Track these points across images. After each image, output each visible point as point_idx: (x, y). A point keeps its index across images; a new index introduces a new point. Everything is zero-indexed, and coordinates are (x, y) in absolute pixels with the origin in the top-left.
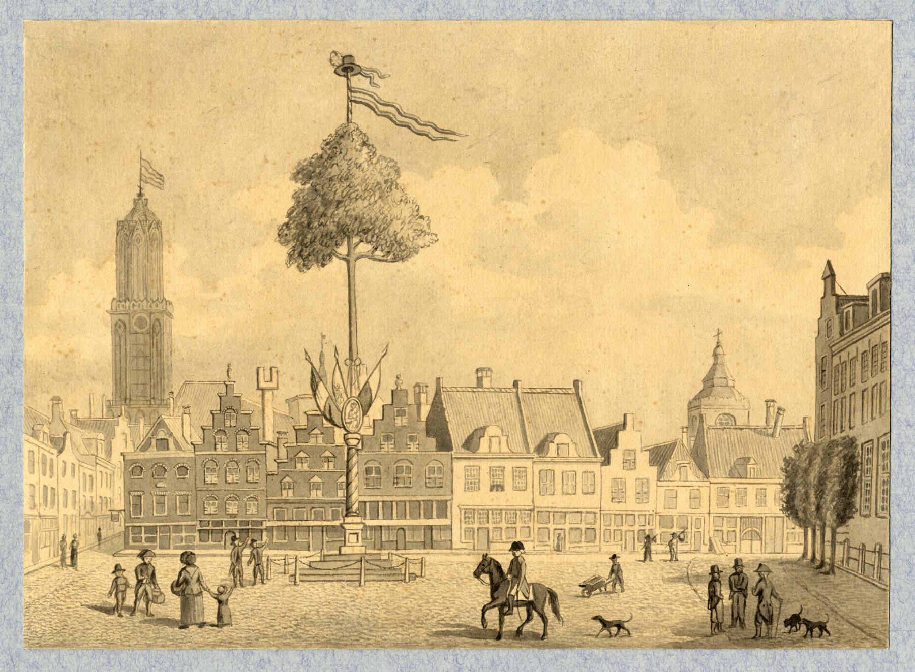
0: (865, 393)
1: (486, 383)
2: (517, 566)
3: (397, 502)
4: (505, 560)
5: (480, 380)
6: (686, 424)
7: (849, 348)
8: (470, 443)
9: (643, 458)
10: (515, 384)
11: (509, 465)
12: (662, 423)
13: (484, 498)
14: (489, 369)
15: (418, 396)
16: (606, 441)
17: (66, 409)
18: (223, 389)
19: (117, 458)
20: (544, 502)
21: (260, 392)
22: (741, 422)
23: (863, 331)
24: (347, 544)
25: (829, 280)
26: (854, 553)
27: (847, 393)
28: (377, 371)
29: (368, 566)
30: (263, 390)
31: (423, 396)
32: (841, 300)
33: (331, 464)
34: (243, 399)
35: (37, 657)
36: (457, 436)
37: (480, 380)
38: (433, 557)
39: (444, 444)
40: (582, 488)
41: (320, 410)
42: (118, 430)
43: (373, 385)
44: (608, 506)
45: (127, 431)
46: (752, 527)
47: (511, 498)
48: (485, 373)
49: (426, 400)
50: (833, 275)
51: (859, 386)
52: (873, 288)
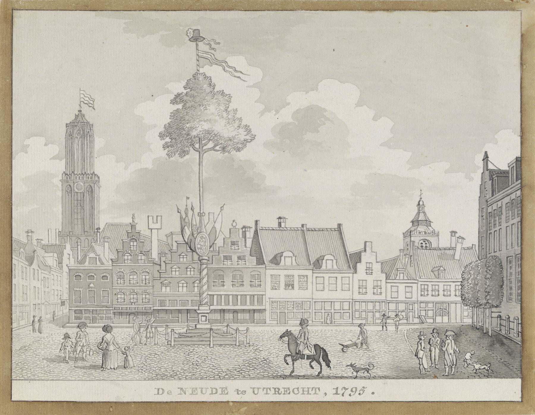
0: (513, 226)
1: (283, 225)
2: (304, 333)
3: (241, 295)
4: (296, 330)
5: (280, 224)
6: (402, 248)
7: (498, 203)
8: (276, 260)
9: (377, 267)
10: (303, 226)
11: (296, 273)
12: (390, 245)
13: (282, 294)
14: (285, 218)
15: (244, 234)
16: (354, 260)
17: (35, 237)
18: (129, 229)
19: (66, 269)
20: (319, 296)
21: (150, 230)
22: (434, 245)
23: (510, 191)
24: (200, 322)
25: (485, 160)
26: (503, 323)
27: (492, 231)
28: (220, 215)
29: (214, 335)
30: (152, 229)
31: (248, 233)
32: (491, 172)
33: (168, 288)
34: (141, 232)
35: (205, 86)
36: (267, 258)
37: (280, 224)
38: (255, 329)
39: (260, 261)
40: (334, 289)
41: (185, 241)
42: (66, 252)
43: (218, 226)
44: (357, 297)
45: (71, 253)
46: (443, 309)
47: (296, 294)
48: (282, 220)
49: (250, 234)
50: (487, 157)
51: (504, 225)
52: (512, 166)
